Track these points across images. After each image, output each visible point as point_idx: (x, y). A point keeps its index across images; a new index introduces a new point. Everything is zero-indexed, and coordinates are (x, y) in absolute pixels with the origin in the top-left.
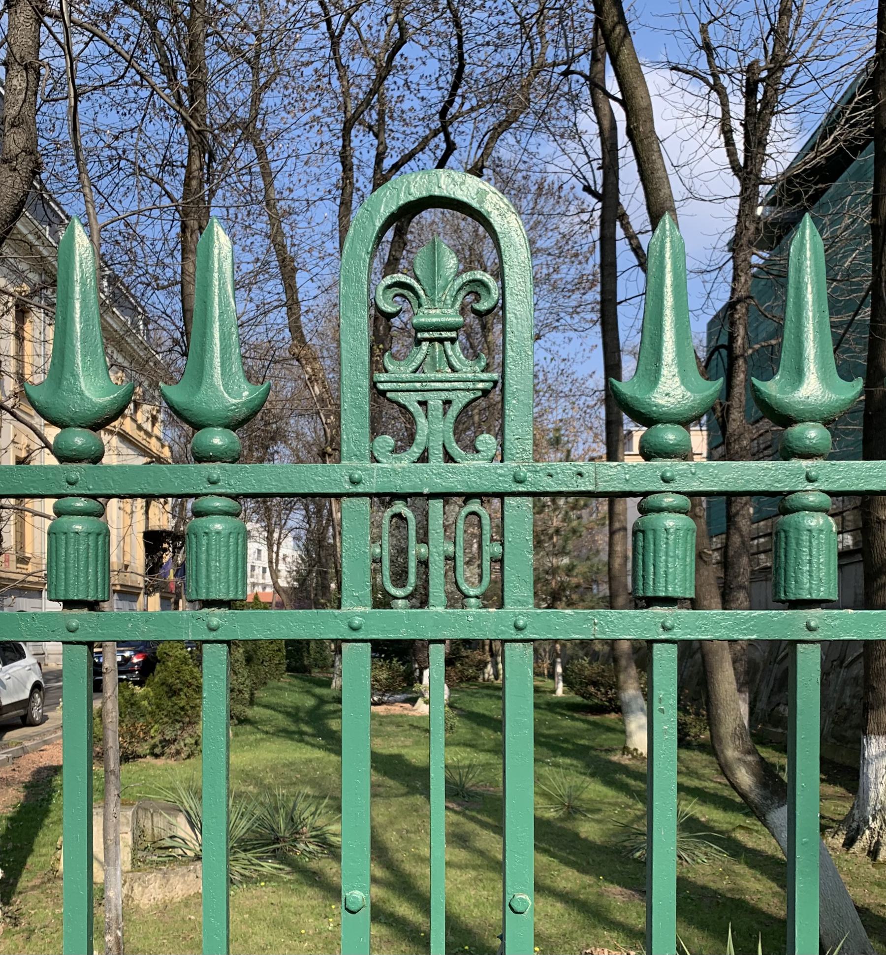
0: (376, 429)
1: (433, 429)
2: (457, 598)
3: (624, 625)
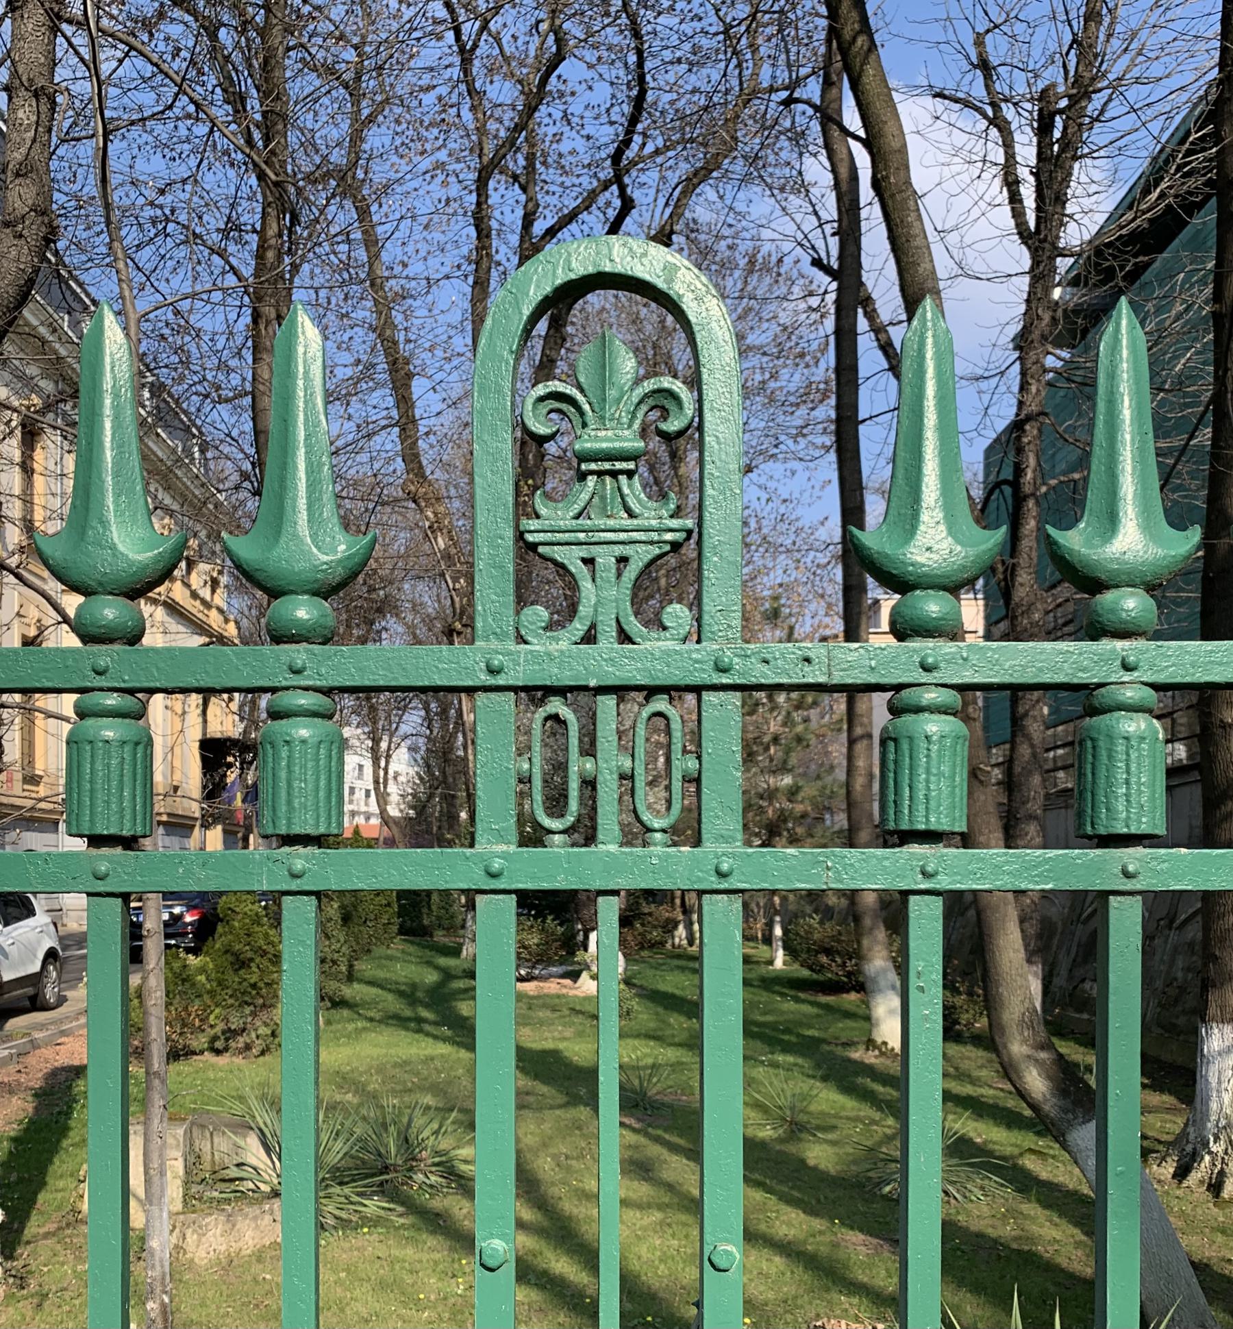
0: (523, 597)
1: (603, 597)
2: (636, 833)
3: (869, 870)
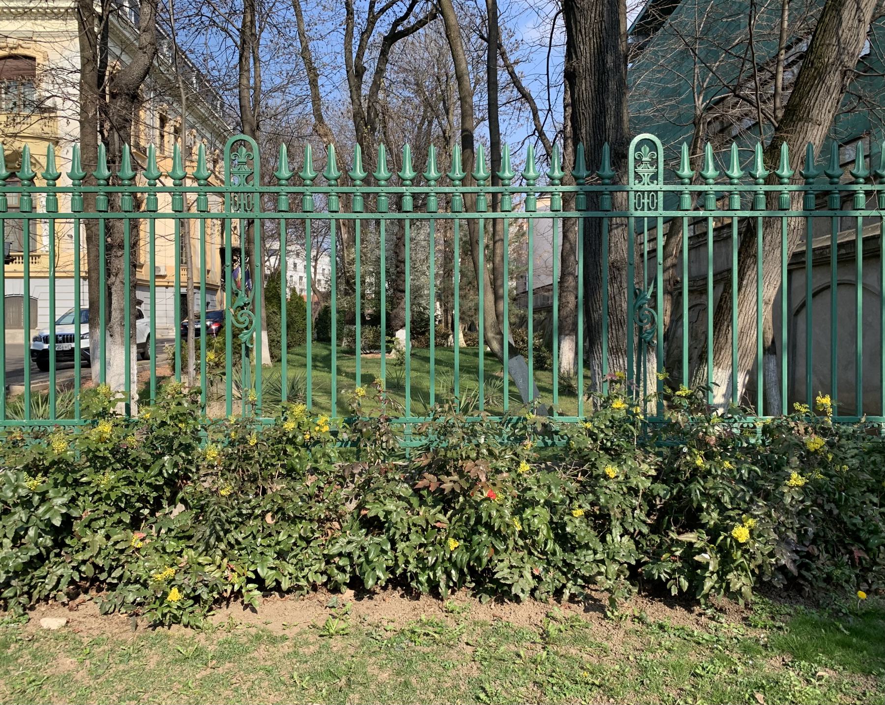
0: (635, 178)
1: (646, 179)
2: (649, 209)
3: (679, 214)
